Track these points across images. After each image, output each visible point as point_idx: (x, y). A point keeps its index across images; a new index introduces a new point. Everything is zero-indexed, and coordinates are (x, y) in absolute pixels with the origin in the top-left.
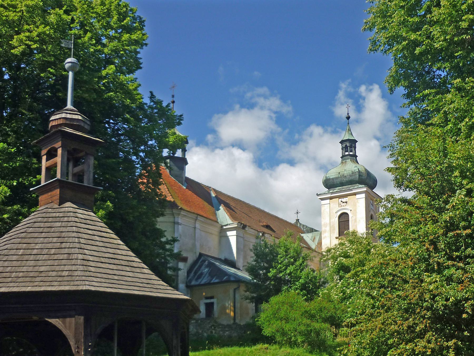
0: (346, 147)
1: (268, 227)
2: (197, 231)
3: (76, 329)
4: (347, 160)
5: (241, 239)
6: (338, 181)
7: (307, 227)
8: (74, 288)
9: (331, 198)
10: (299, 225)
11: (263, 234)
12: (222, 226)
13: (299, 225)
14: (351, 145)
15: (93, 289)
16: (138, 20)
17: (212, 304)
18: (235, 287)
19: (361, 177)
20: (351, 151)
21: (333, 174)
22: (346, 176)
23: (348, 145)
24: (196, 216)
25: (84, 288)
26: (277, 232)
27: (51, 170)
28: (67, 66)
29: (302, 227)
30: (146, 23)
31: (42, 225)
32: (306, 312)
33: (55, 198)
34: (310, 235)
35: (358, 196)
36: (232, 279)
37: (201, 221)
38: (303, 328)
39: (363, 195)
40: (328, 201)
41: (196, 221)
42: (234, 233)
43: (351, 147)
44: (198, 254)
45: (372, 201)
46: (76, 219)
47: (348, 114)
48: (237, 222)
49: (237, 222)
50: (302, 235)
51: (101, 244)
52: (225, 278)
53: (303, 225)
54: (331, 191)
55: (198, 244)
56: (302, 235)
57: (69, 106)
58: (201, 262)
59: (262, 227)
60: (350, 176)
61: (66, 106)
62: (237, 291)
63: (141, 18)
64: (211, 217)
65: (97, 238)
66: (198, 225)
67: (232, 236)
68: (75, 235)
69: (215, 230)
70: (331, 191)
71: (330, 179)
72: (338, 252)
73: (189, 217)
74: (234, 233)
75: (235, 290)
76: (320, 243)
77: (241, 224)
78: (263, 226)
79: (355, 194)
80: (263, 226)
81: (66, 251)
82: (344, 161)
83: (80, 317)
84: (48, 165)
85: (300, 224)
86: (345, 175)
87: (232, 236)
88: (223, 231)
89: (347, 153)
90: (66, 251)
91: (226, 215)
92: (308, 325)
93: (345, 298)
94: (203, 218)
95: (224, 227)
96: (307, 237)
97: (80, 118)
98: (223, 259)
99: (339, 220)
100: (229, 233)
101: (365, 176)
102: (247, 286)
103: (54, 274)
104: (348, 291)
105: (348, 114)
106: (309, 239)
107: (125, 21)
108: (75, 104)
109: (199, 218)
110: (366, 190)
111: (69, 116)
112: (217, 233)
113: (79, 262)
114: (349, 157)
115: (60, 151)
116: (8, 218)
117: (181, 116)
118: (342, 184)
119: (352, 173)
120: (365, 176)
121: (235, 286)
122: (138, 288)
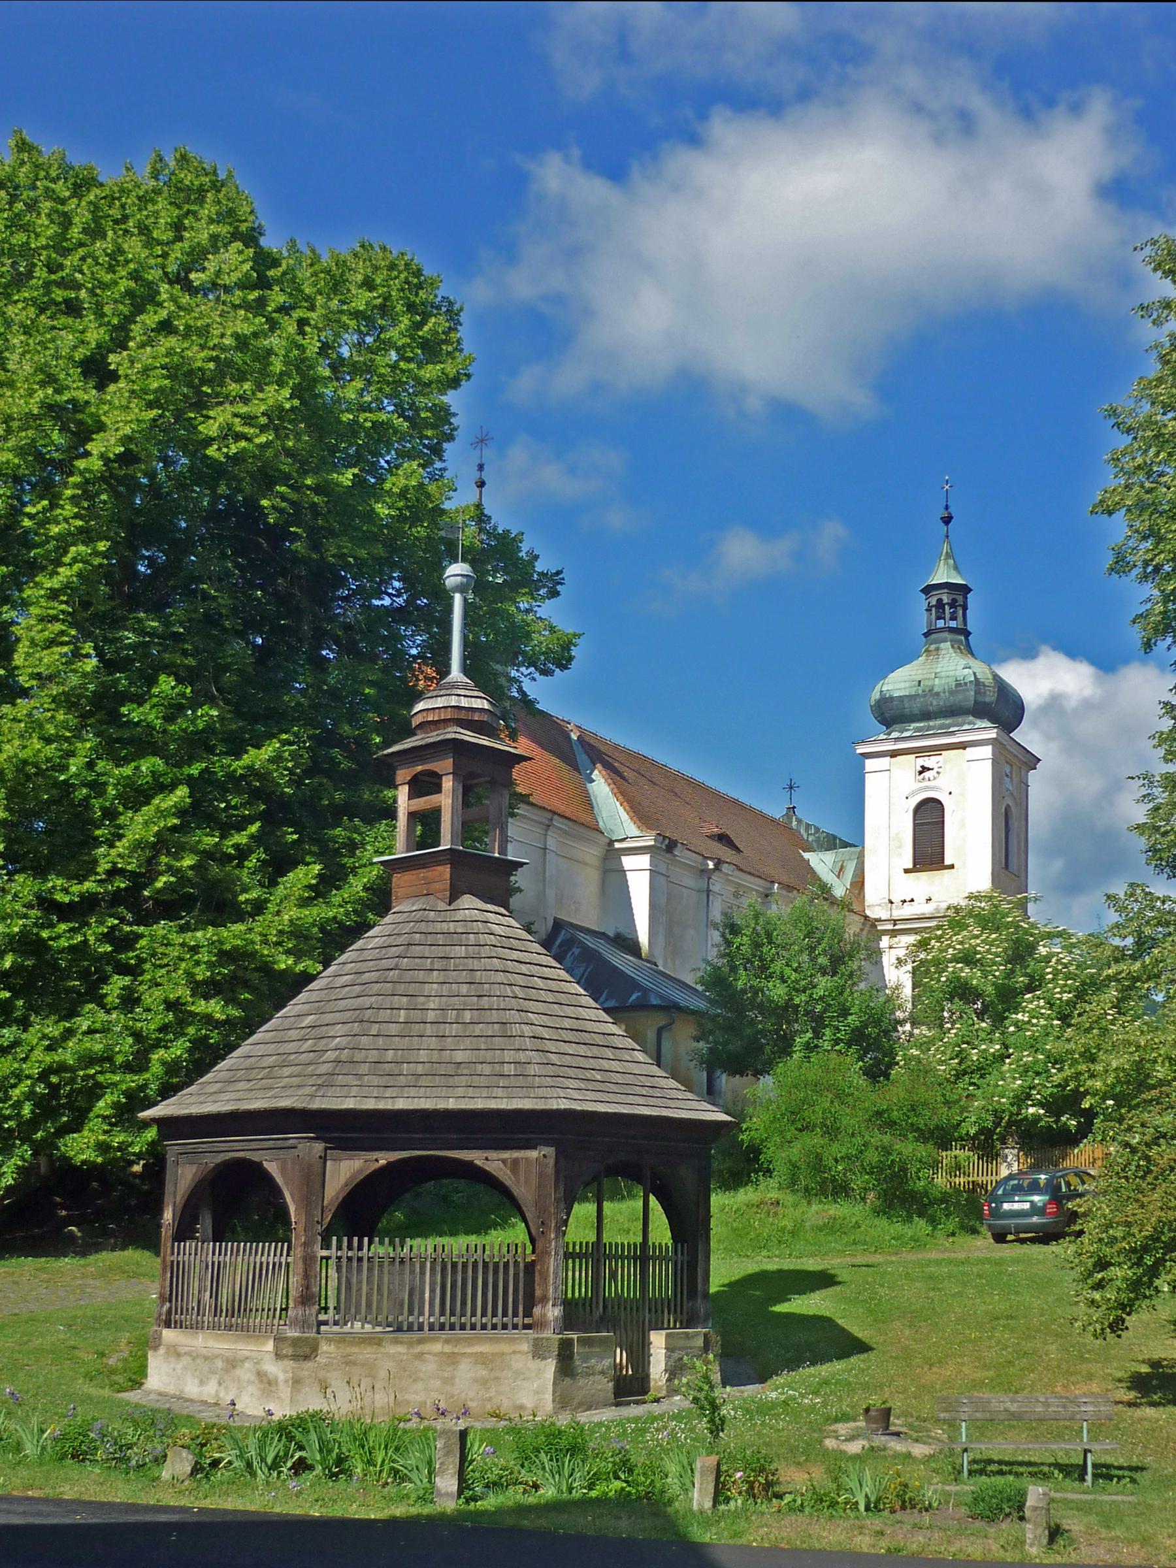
0: (940, 605)
1: (723, 839)
2: (550, 857)
3: (540, 1186)
4: (942, 645)
5: (663, 880)
6: (916, 706)
7: (817, 830)
8: (540, 1105)
9: (894, 754)
10: (794, 823)
11: (719, 863)
12: (611, 842)
13: (794, 823)
14: (954, 601)
15: (577, 1107)
16: (444, 309)
17: (1082, 1479)
18: (662, 1023)
19: (980, 699)
20: (953, 618)
21: (902, 685)
22: (938, 694)
23: (945, 601)
24: (549, 815)
25: (564, 1105)
26: (747, 852)
27: (427, 821)
28: (450, 582)
29: (802, 831)
30: (463, 318)
31: (426, 951)
32: (879, 1114)
33: (437, 886)
34: (829, 857)
35: (971, 752)
36: (655, 1001)
37: (560, 829)
38: (872, 1156)
39: (987, 751)
40: (884, 762)
41: (546, 830)
42: (644, 861)
43: (953, 604)
44: (550, 923)
45: (1013, 767)
46: (492, 940)
47: (947, 508)
48: (654, 833)
49: (654, 833)
50: (806, 855)
51: (550, 997)
52: (634, 997)
53: (808, 826)
54: (895, 735)
55: (551, 894)
56: (806, 855)
57: (456, 673)
58: (560, 946)
59: (709, 841)
60: (951, 692)
61: (448, 673)
62: (665, 1035)
63: (451, 304)
64: (584, 817)
65: (540, 983)
66: (551, 843)
67: (638, 874)
68: (501, 977)
69: (591, 853)
70: (895, 735)
71: (891, 698)
72: (951, 951)
73: (529, 819)
74: (644, 861)
75: (660, 1031)
76: (859, 884)
77: (665, 837)
78: (711, 837)
79: (963, 746)
80: (711, 837)
81: (494, 1016)
82: (933, 647)
83: (714, 1209)
84: (413, 809)
85: (799, 821)
86: (936, 689)
87: (638, 874)
88: (611, 856)
89: (941, 623)
90: (494, 1016)
91: (621, 809)
92: (887, 1151)
93: (965, 1073)
94: (566, 821)
95: (617, 845)
96: (821, 863)
97: (486, 706)
98: (611, 934)
99: (914, 820)
100: (628, 862)
101: (991, 697)
102: (700, 1025)
103: (487, 1069)
104: (974, 1055)
105: (947, 508)
106: (826, 870)
107: (426, 328)
108: (466, 670)
109: (558, 822)
110: (994, 736)
111: (464, 703)
112: (595, 862)
113: (528, 1043)
114: (946, 635)
115: (448, 783)
116: (191, 868)
117: (558, 573)
118: (926, 716)
119: (957, 685)
120: (991, 697)
121: (660, 1020)
122: (641, 1100)
